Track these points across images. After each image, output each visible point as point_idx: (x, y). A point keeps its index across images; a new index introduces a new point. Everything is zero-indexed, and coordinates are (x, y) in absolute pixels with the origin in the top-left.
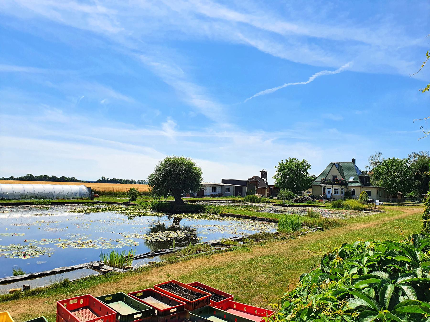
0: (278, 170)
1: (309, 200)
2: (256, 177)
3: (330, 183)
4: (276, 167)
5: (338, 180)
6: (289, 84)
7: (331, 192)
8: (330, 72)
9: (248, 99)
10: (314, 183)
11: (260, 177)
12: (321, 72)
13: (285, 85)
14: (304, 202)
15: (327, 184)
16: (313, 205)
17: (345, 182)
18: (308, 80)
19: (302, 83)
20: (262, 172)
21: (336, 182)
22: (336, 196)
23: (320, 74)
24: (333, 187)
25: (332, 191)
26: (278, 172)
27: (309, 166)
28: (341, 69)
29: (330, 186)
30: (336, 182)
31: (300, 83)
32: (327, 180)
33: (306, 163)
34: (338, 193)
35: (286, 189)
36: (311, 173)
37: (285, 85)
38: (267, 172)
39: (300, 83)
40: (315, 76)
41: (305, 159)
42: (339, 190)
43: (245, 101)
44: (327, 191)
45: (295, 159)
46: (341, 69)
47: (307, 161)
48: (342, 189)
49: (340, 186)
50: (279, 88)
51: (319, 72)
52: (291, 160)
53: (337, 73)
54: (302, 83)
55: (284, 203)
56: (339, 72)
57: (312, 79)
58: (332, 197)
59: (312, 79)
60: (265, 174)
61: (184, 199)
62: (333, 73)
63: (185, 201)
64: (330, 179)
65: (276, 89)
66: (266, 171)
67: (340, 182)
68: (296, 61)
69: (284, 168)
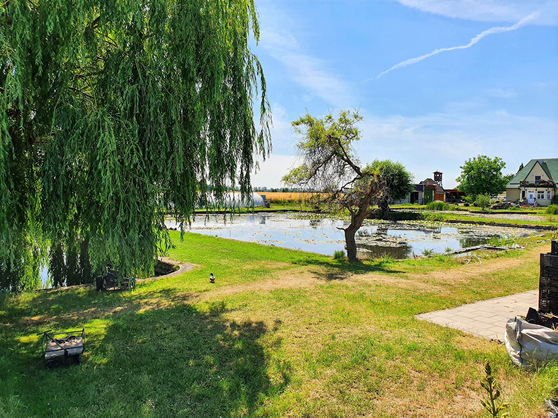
0: (463, 170)
1: (512, 206)
2: (430, 180)
3: (532, 186)
4: (461, 167)
5: (543, 182)
6: (442, 50)
7: (534, 196)
8: (503, 28)
9: (383, 73)
10: (508, 186)
11: (433, 179)
12: (490, 29)
13: (436, 52)
14: (505, 209)
15: (528, 186)
16: (519, 211)
17: (552, 185)
18: (470, 42)
19: (460, 47)
20: (436, 173)
21: (539, 183)
22: (541, 201)
23: (488, 32)
24: (536, 190)
25: (535, 195)
26: (463, 174)
27: (503, 164)
28: (520, 23)
29: (533, 189)
30: (539, 183)
31: (457, 48)
32: (528, 182)
33: (500, 161)
34: (543, 197)
35: (486, 194)
36: (505, 173)
37: (436, 52)
38: (441, 174)
39: (457, 48)
40: (480, 36)
41: (499, 157)
42: (545, 194)
43: (379, 76)
44: (527, 195)
45: (485, 157)
46: (520, 23)
47: (501, 159)
48: (549, 192)
49: (547, 189)
50: (428, 55)
51: (487, 30)
52: (479, 158)
53: (514, 29)
54: (460, 47)
55: (483, 210)
56: (517, 27)
57: (474, 41)
58: (537, 202)
59: (474, 41)
60: (440, 175)
61: (391, 207)
62: (509, 29)
63: (391, 209)
64: (532, 180)
65: (422, 58)
66: (441, 172)
67: (546, 184)
68: (454, 16)
69: (472, 168)
